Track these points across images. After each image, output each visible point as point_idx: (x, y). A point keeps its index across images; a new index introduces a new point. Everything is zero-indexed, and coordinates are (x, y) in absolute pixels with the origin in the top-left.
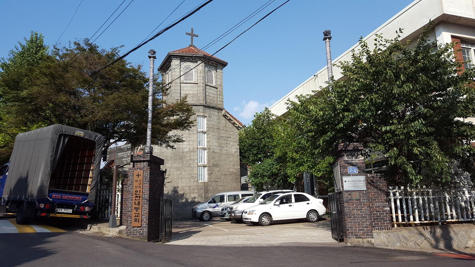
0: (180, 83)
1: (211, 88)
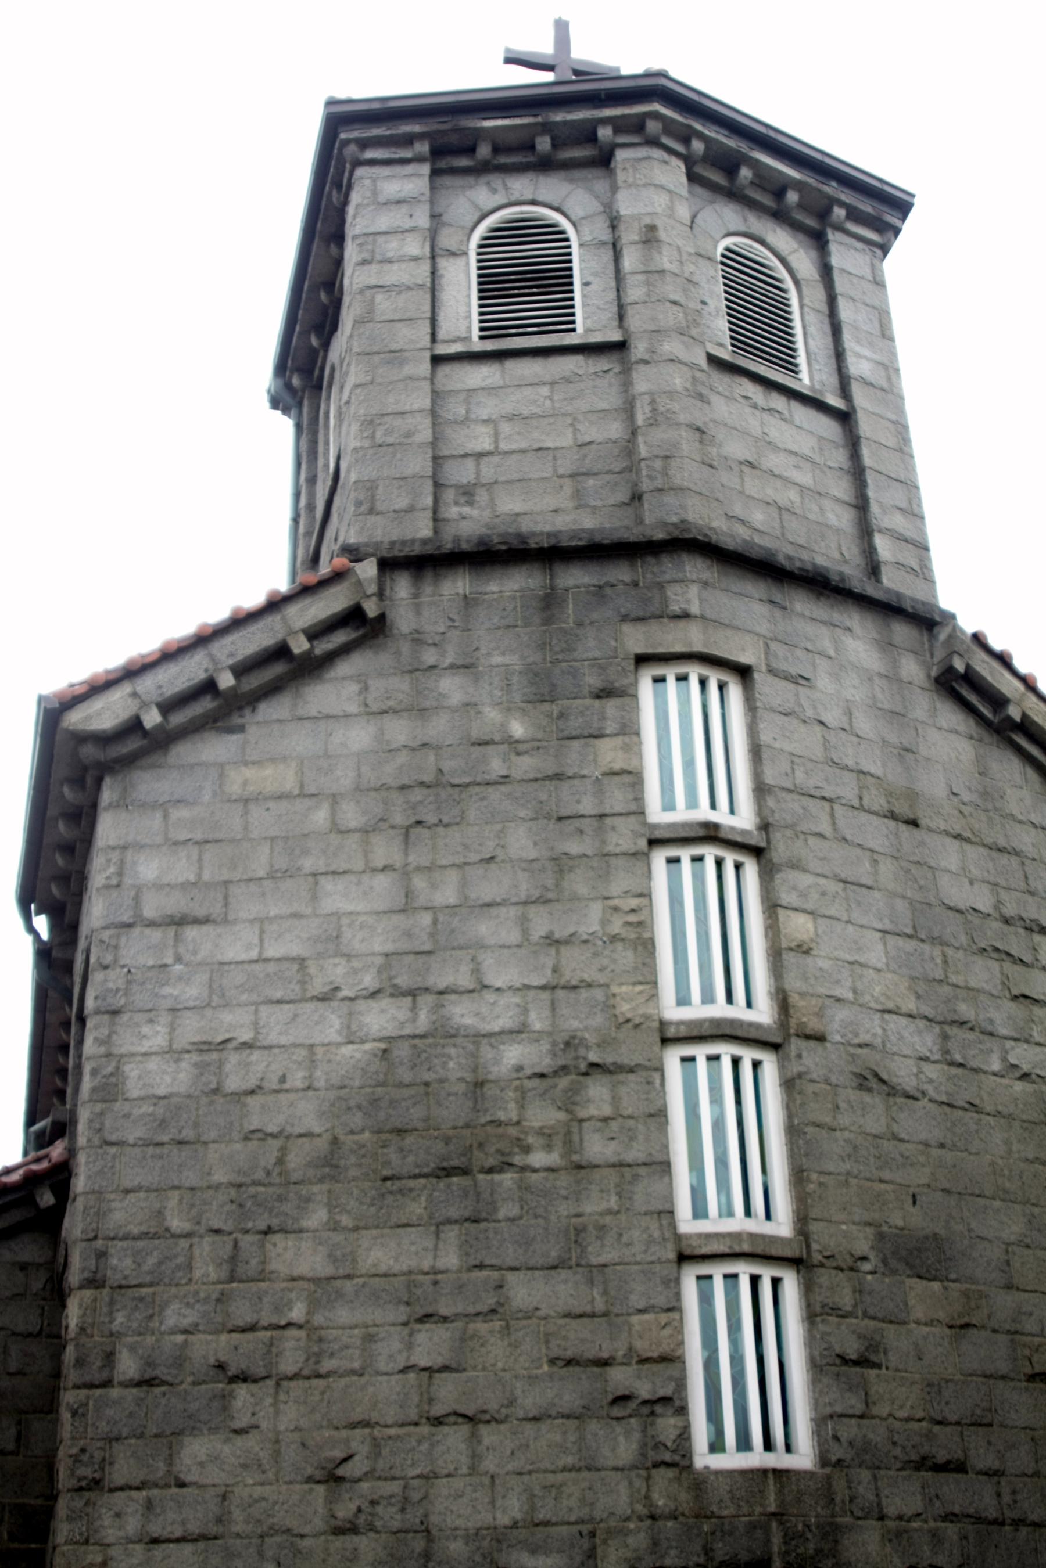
1: (779, 402)
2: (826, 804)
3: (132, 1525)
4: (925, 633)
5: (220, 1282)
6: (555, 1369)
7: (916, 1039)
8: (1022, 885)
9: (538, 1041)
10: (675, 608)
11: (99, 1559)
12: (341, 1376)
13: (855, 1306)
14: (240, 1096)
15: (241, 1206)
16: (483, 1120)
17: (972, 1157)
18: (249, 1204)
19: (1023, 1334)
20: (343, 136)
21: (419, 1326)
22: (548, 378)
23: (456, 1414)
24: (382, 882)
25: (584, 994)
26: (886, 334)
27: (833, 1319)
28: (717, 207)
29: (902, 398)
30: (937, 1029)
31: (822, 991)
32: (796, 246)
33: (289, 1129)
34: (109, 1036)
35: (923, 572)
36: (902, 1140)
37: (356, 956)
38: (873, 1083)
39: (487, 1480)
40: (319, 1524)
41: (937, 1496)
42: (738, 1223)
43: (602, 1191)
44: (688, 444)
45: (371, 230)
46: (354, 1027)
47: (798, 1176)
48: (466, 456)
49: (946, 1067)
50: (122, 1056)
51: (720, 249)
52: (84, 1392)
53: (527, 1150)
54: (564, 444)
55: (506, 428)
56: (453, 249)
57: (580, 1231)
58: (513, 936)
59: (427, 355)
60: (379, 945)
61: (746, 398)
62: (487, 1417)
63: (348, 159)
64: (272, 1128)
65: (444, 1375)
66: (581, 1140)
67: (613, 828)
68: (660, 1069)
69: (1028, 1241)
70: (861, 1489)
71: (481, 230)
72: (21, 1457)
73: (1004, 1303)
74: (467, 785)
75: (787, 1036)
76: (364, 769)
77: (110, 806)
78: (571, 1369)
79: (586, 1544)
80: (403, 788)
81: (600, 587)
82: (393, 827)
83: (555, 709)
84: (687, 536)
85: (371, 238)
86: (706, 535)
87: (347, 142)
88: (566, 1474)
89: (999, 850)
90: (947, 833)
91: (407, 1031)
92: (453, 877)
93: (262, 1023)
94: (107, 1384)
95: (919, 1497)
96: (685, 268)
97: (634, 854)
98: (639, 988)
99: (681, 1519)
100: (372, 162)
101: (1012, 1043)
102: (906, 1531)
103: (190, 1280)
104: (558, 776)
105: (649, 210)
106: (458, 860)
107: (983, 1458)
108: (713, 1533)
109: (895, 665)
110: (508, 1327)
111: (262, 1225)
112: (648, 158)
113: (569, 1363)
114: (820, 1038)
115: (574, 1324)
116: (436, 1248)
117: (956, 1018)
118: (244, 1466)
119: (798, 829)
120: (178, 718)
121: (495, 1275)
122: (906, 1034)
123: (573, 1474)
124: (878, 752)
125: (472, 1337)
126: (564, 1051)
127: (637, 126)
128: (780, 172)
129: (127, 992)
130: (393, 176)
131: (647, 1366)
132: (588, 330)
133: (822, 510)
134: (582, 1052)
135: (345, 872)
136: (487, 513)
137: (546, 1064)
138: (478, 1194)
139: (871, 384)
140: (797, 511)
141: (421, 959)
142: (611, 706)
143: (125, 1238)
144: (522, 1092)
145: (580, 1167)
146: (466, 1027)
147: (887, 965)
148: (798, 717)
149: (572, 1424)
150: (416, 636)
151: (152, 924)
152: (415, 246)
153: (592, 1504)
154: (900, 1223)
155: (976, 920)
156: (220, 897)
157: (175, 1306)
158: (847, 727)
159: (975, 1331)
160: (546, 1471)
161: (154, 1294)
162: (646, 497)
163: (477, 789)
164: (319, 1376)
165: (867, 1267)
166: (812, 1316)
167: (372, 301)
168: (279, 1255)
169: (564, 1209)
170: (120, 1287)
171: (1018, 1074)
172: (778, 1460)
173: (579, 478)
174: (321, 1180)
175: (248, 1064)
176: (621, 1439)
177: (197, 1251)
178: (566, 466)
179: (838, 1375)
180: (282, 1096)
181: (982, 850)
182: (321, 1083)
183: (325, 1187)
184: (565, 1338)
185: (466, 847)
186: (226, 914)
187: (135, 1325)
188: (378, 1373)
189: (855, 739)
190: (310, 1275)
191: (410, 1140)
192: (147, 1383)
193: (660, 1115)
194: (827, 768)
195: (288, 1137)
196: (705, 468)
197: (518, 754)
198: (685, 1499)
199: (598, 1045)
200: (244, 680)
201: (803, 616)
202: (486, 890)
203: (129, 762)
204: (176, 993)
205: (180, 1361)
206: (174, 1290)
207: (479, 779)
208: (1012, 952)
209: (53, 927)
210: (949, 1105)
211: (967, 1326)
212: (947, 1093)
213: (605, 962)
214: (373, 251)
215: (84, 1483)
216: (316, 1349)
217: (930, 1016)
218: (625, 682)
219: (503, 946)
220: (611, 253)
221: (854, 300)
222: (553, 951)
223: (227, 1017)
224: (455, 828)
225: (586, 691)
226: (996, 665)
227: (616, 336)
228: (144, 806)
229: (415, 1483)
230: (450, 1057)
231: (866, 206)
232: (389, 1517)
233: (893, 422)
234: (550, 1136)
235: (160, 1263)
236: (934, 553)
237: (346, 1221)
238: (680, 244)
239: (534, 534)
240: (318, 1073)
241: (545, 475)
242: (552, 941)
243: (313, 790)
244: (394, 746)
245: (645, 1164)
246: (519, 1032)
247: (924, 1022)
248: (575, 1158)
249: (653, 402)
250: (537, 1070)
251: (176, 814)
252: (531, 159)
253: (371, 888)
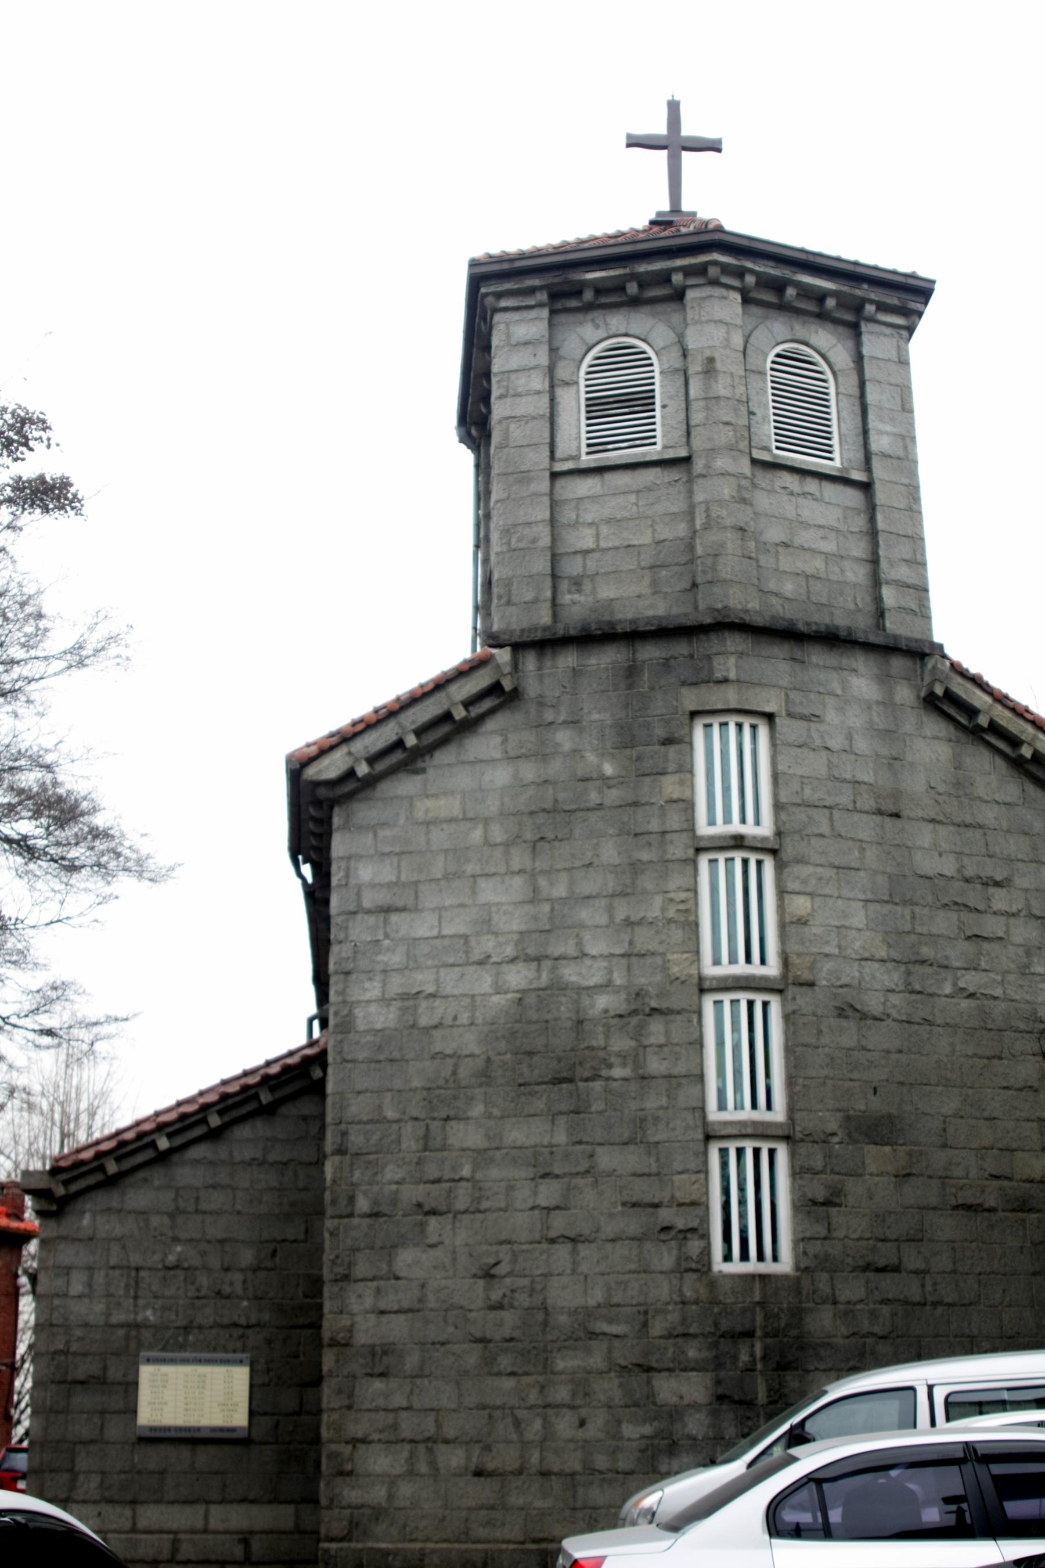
0: (554, 476)
1: (812, 485)
2: (826, 811)
3: (368, 1302)
4: (918, 662)
5: (418, 1151)
6: (626, 1209)
7: (885, 977)
8: (983, 851)
9: (618, 992)
10: (718, 675)
11: (349, 1323)
12: (494, 1211)
13: (825, 1166)
14: (428, 1030)
15: (430, 1102)
16: (582, 1046)
17: (923, 1058)
18: (435, 1101)
19: (951, 1178)
20: (483, 290)
21: (540, 1181)
22: (635, 488)
23: (563, 1236)
24: (518, 881)
25: (649, 960)
26: (906, 408)
27: (809, 1176)
28: (768, 323)
29: (916, 462)
30: (903, 968)
31: (814, 950)
32: (834, 342)
33: (459, 1052)
34: (344, 989)
35: (922, 613)
36: (869, 1050)
37: (501, 934)
38: (850, 1012)
39: (582, 1278)
40: (480, 1303)
41: (877, 1288)
42: (746, 1114)
43: (657, 1094)
44: (732, 543)
45: (505, 369)
46: (500, 983)
47: (790, 1082)
48: (576, 553)
49: (907, 995)
50: (353, 1002)
51: (771, 357)
52: (336, 1221)
53: (610, 1066)
54: (646, 542)
55: (604, 530)
56: (567, 379)
57: (643, 1120)
58: (604, 920)
59: (547, 474)
60: (516, 926)
61: (785, 488)
62: (582, 1239)
63: (488, 307)
64: (449, 1051)
65: (557, 1212)
66: (645, 1060)
67: (671, 842)
69: (962, 1113)
70: (821, 1286)
71: (588, 360)
73: (939, 1158)
74: (574, 811)
75: (787, 985)
76: (506, 799)
77: (339, 828)
78: (635, 1209)
79: (642, 1318)
80: (532, 813)
81: (667, 659)
82: (525, 842)
83: (634, 753)
84: (727, 620)
85: (506, 375)
86: (741, 618)
87: (486, 295)
88: (631, 1276)
89: (966, 826)
90: (924, 819)
91: (534, 986)
92: (564, 876)
93: (441, 980)
94: (351, 1215)
95: (863, 1289)
96: (737, 391)
97: (685, 860)
98: (685, 956)
99: (701, 1304)
100: (506, 309)
101: (963, 972)
102: (852, 1311)
103: (400, 1150)
104: (635, 804)
105: (710, 343)
106: (568, 865)
107: (912, 1260)
108: (720, 1313)
109: (891, 693)
110: (596, 1181)
111: (443, 1114)
112: (711, 296)
113: (634, 1205)
114: (811, 984)
115: (638, 1180)
116: (552, 1130)
117: (919, 958)
118: (435, 1267)
119: (804, 833)
120: (381, 766)
121: (589, 1148)
122: (878, 975)
123: (635, 1275)
124: (871, 765)
125: (574, 1188)
126: (635, 999)
127: (701, 270)
128: (820, 287)
129: (354, 959)
130: (522, 320)
131: (683, 1208)
132: (665, 447)
133: (842, 571)
134: (647, 1000)
135: (494, 875)
136: (590, 599)
137: (623, 1008)
138: (579, 1096)
139: (890, 456)
140: (822, 576)
141: (544, 936)
142: (672, 751)
143: (359, 1122)
144: (608, 1028)
145: (643, 1078)
146: (573, 983)
147: (867, 925)
148: (809, 747)
149: (635, 1243)
150: (540, 699)
151: (369, 912)
152: (538, 382)
153: (647, 1294)
154: (863, 1108)
155: (941, 882)
156: (412, 893)
157: (391, 1167)
158: (848, 748)
159: (915, 1178)
160: (618, 1273)
161: (377, 1159)
162: (701, 587)
163: (581, 814)
164: (479, 1211)
165: (836, 1139)
166: (795, 1173)
167: (508, 428)
168: (454, 1134)
169: (634, 1105)
170: (357, 1154)
171: (965, 994)
172: (768, 1267)
173: (656, 570)
174: (480, 1085)
175: (433, 1008)
176: (665, 1254)
177: (403, 1131)
178: (646, 560)
179: (809, 1212)
180: (455, 1030)
181: (951, 828)
182: (479, 1021)
183: (483, 1090)
184: (632, 1189)
185: (573, 856)
186: (417, 904)
187: (366, 1178)
188: (516, 1210)
189: (853, 757)
190: (474, 1147)
191: (536, 1059)
192: (375, 1215)
193: (699, 1043)
194: (830, 784)
195: (459, 1057)
196: (746, 561)
197: (609, 787)
198: (703, 1292)
199: (657, 996)
201: (818, 665)
202: (587, 887)
203: (350, 796)
204: (386, 959)
205: (394, 1202)
206: (389, 1156)
207: (582, 807)
208: (969, 904)
209: (315, 874)
210: (908, 1022)
211: (908, 1175)
212: (907, 1014)
213: (664, 937)
214: (508, 387)
215: (338, 1277)
216: (477, 1195)
217: (898, 959)
218: (683, 732)
219: (597, 927)
220: (682, 378)
221: (879, 382)
222: (629, 930)
223: (419, 976)
224: (566, 842)
225: (655, 739)
226: (969, 686)
227: (683, 453)
228: (362, 828)
229: (539, 1279)
230: (561, 1003)
231: (893, 299)
232: (523, 1299)
233: (906, 486)
234: (625, 1057)
235: (381, 1140)
236: (932, 594)
237: (496, 1112)
238: (733, 370)
239: (620, 621)
240: (478, 1014)
241: (632, 567)
242: (629, 923)
243: (471, 815)
244: (525, 782)
245: (685, 1076)
246: (607, 986)
247: (893, 964)
248: (641, 1072)
249: (707, 509)
250: (618, 1012)
251: (383, 833)
252: (624, 299)
253: (511, 886)
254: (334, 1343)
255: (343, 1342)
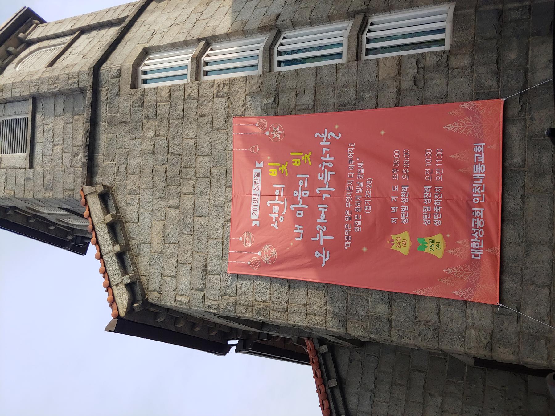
68: (279, 73)
72: (428, 371)
94: (390, 321)
200: (120, 242)
215: (435, 336)
227: (31, 101)
254: (490, 346)
255: (489, 339)
